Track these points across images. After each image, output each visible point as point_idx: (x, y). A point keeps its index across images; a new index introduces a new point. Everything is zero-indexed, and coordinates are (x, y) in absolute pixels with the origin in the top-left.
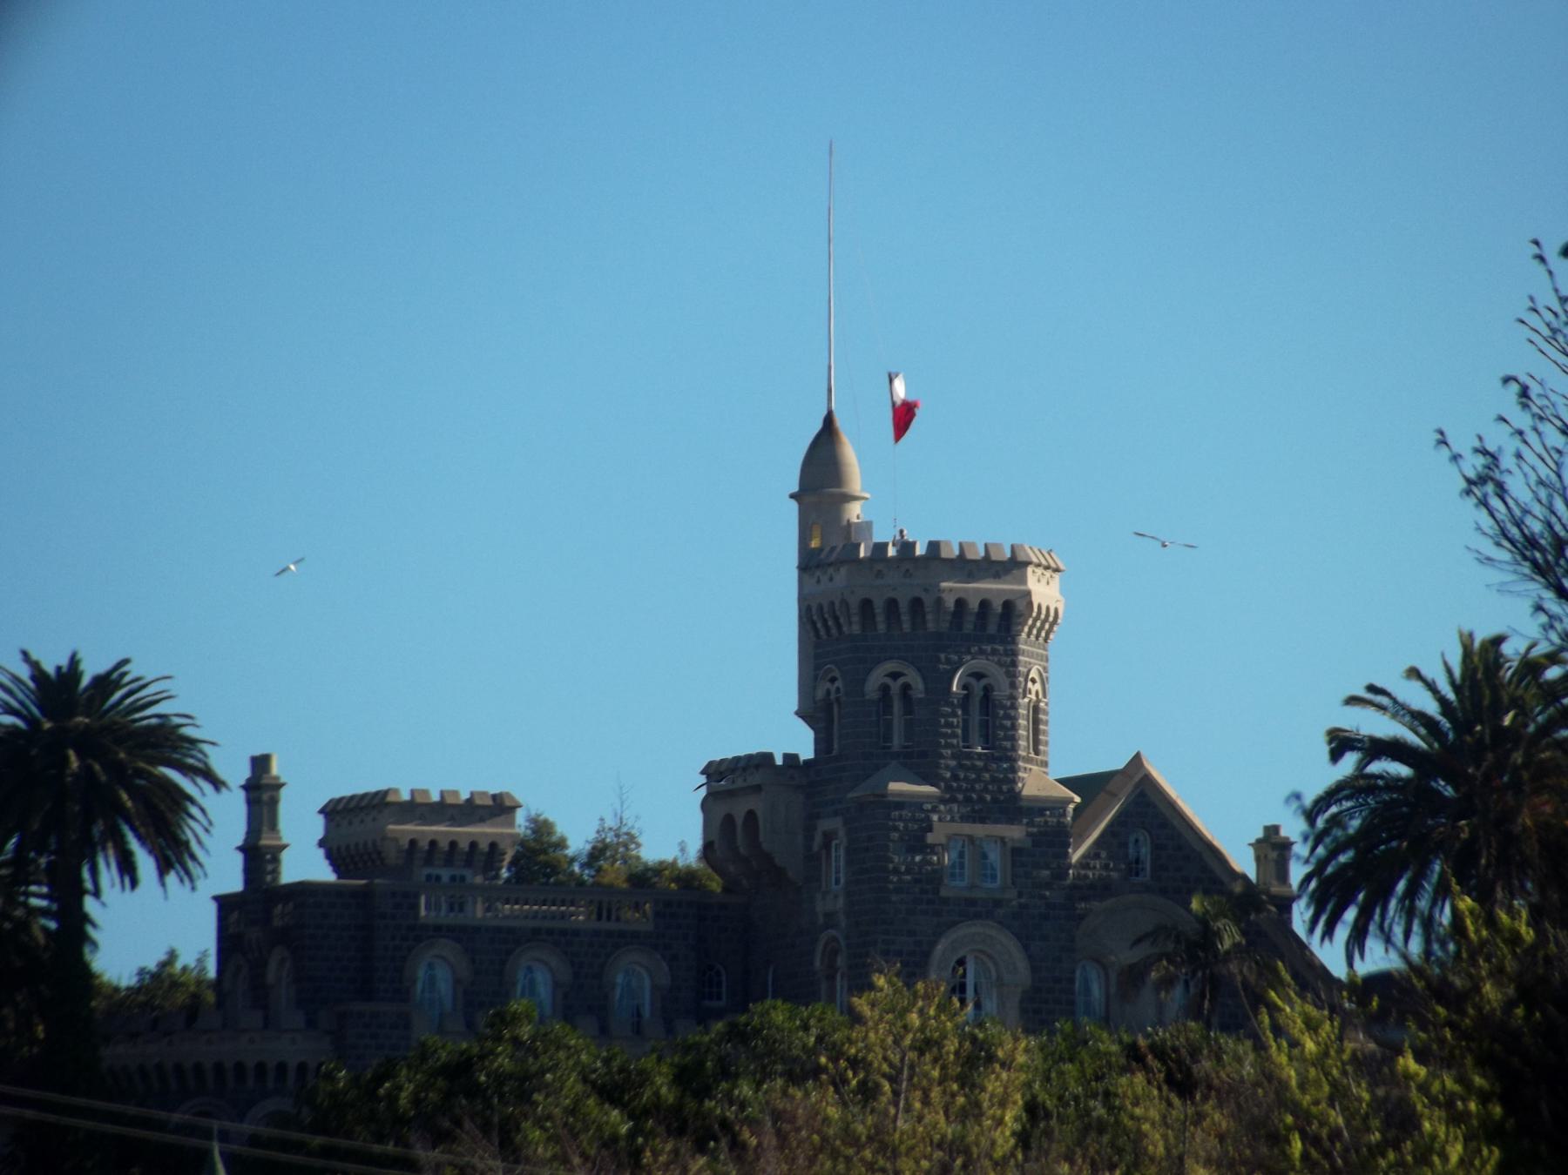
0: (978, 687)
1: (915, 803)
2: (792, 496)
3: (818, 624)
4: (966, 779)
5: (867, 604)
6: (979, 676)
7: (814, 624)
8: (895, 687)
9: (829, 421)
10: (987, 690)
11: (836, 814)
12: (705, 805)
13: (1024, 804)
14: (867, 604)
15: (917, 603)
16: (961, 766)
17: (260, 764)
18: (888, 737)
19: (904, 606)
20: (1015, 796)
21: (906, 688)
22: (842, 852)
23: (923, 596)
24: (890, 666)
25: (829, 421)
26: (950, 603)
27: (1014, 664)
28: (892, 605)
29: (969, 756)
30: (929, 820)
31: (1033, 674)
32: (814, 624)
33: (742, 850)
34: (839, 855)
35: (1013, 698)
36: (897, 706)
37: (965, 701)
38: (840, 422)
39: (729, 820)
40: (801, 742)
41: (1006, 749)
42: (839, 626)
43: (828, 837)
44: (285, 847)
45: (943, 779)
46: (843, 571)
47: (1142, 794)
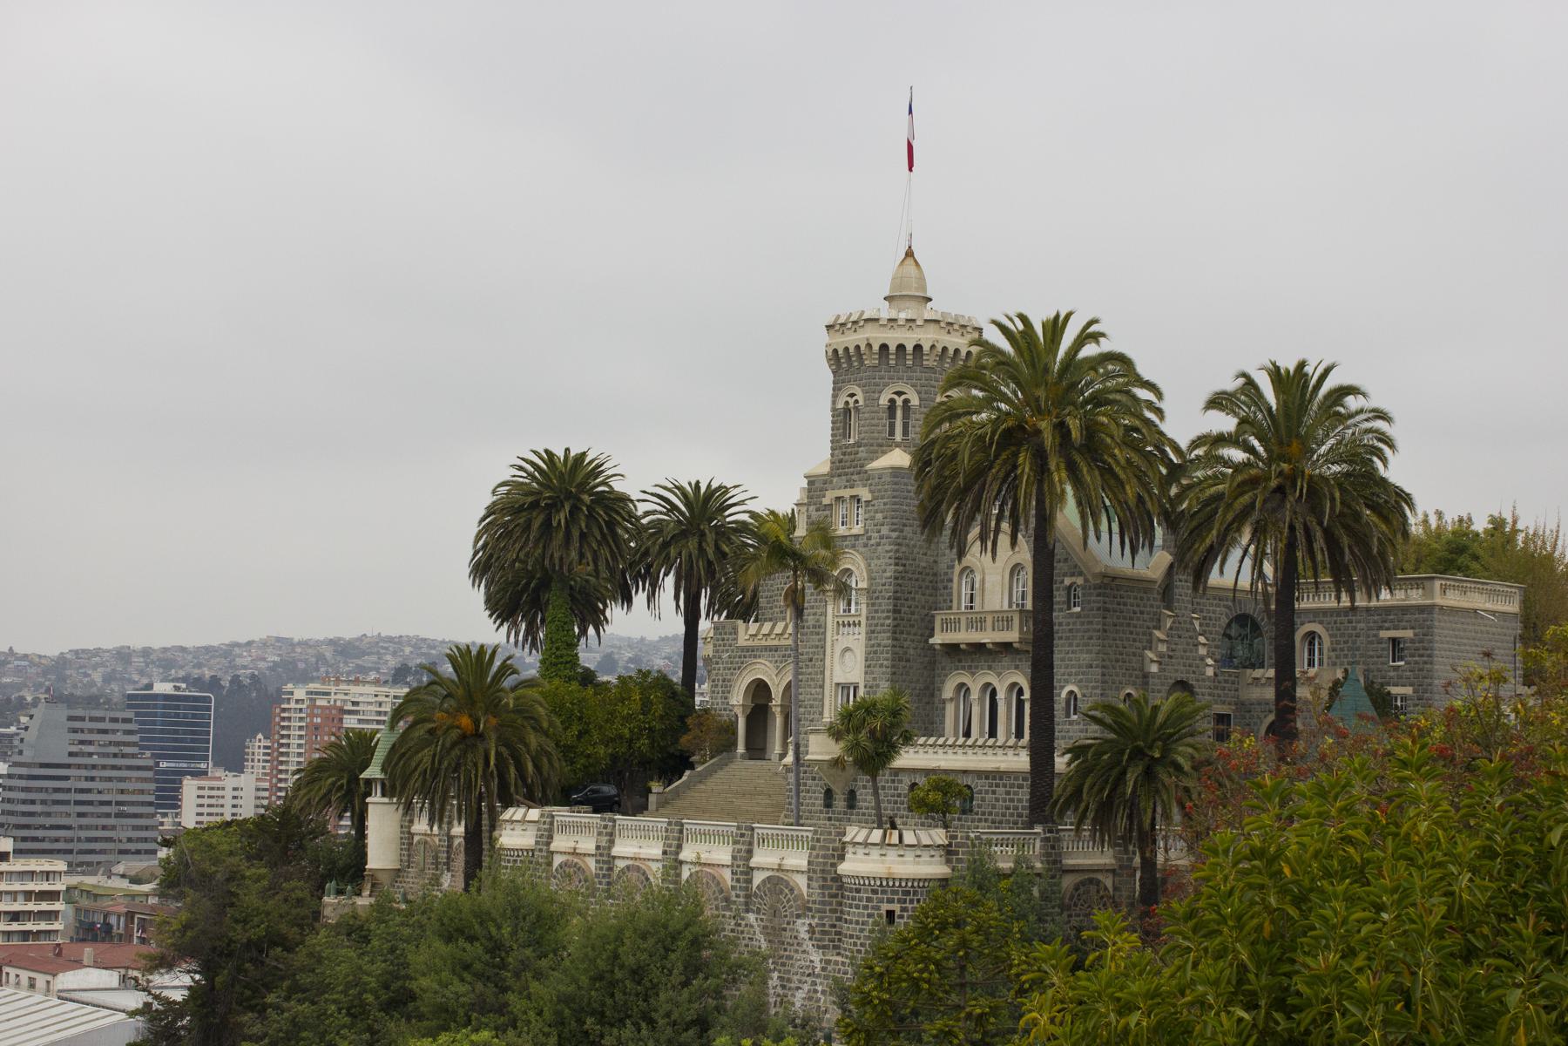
5: (884, 347)
6: (899, 393)
8: (899, 401)
18: (892, 433)
21: (906, 401)
25: (910, 254)
28: (901, 347)
36: (899, 413)
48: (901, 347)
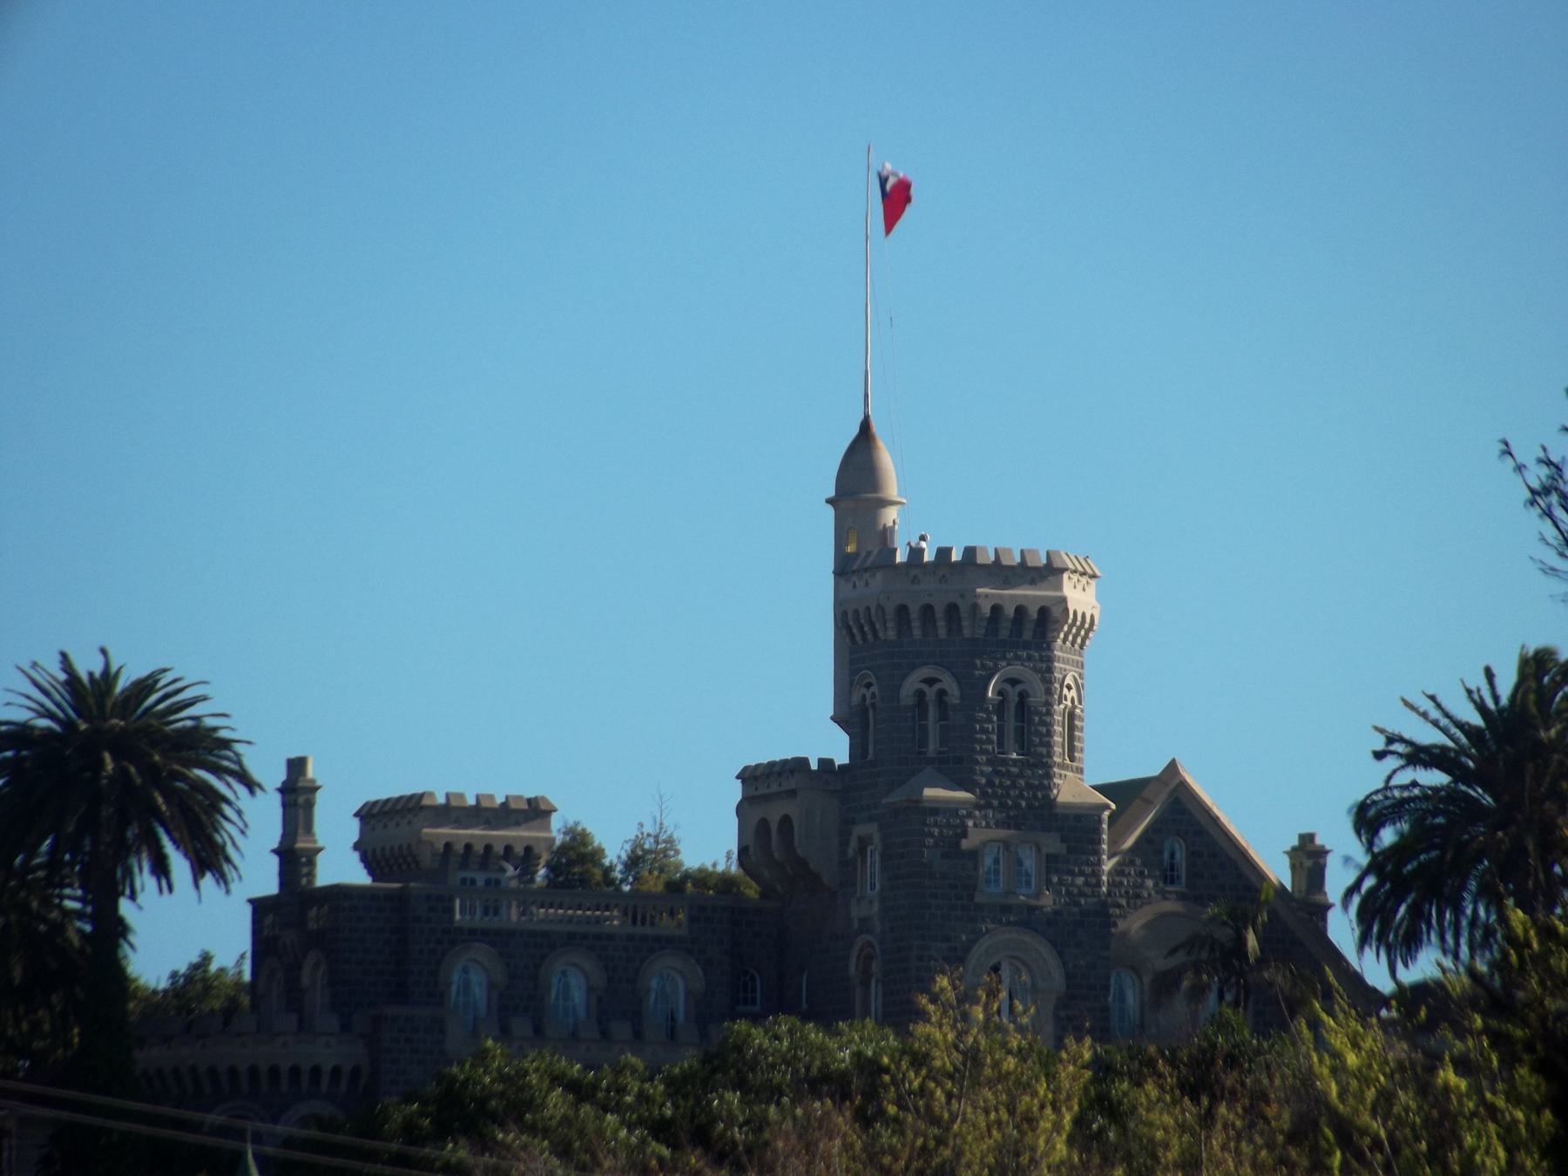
0: (1013, 693)
1: (951, 809)
2: (829, 501)
3: (854, 630)
4: (1001, 785)
5: (902, 610)
6: (1014, 682)
7: (849, 629)
8: (931, 693)
9: (866, 427)
10: (1023, 696)
11: (871, 819)
12: (740, 810)
13: (1059, 811)
14: (902, 610)
15: (952, 609)
16: (997, 772)
17: (296, 766)
18: (923, 742)
19: (939, 612)
20: (1051, 803)
21: (942, 693)
22: (877, 858)
23: (960, 603)
24: (926, 672)
25: (866, 427)
26: (986, 610)
27: (1050, 670)
29: (1004, 762)
30: (965, 827)
31: (1069, 680)
32: (849, 629)
33: (776, 855)
34: (874, 860)
35: (1049, 704)
36: (932, 713)
37: (1001, 708)
38: (876, 427)
39: (763, 825)
40: (836, 747)
41: (1041, 755)
42: (875, 632)
43: (864, 842)
44: (320, 850)
45: (978, 784)
46: (879, 576)
47: (1177, 801)
48: (928, 610)
